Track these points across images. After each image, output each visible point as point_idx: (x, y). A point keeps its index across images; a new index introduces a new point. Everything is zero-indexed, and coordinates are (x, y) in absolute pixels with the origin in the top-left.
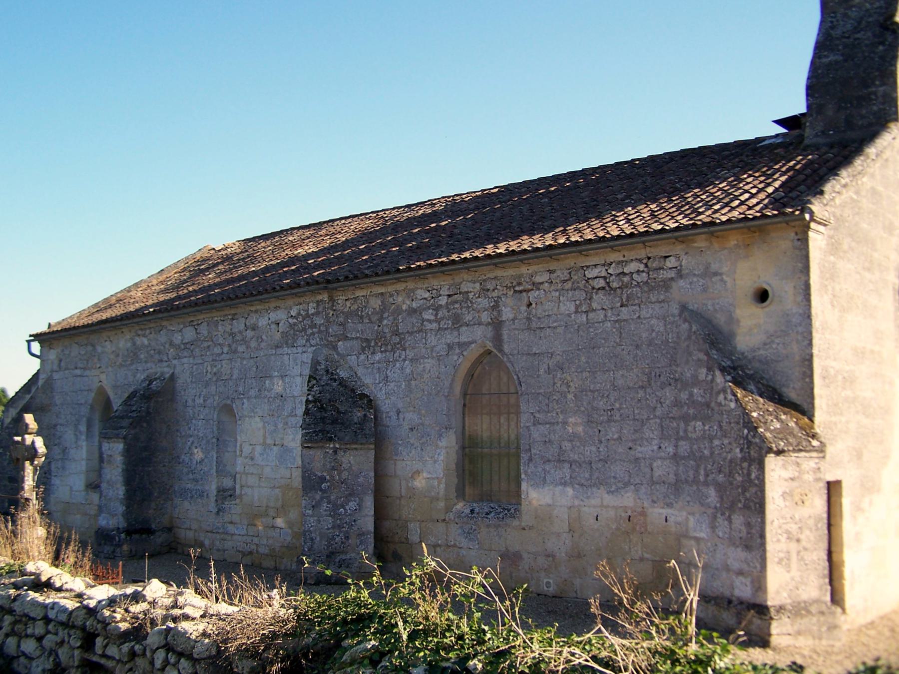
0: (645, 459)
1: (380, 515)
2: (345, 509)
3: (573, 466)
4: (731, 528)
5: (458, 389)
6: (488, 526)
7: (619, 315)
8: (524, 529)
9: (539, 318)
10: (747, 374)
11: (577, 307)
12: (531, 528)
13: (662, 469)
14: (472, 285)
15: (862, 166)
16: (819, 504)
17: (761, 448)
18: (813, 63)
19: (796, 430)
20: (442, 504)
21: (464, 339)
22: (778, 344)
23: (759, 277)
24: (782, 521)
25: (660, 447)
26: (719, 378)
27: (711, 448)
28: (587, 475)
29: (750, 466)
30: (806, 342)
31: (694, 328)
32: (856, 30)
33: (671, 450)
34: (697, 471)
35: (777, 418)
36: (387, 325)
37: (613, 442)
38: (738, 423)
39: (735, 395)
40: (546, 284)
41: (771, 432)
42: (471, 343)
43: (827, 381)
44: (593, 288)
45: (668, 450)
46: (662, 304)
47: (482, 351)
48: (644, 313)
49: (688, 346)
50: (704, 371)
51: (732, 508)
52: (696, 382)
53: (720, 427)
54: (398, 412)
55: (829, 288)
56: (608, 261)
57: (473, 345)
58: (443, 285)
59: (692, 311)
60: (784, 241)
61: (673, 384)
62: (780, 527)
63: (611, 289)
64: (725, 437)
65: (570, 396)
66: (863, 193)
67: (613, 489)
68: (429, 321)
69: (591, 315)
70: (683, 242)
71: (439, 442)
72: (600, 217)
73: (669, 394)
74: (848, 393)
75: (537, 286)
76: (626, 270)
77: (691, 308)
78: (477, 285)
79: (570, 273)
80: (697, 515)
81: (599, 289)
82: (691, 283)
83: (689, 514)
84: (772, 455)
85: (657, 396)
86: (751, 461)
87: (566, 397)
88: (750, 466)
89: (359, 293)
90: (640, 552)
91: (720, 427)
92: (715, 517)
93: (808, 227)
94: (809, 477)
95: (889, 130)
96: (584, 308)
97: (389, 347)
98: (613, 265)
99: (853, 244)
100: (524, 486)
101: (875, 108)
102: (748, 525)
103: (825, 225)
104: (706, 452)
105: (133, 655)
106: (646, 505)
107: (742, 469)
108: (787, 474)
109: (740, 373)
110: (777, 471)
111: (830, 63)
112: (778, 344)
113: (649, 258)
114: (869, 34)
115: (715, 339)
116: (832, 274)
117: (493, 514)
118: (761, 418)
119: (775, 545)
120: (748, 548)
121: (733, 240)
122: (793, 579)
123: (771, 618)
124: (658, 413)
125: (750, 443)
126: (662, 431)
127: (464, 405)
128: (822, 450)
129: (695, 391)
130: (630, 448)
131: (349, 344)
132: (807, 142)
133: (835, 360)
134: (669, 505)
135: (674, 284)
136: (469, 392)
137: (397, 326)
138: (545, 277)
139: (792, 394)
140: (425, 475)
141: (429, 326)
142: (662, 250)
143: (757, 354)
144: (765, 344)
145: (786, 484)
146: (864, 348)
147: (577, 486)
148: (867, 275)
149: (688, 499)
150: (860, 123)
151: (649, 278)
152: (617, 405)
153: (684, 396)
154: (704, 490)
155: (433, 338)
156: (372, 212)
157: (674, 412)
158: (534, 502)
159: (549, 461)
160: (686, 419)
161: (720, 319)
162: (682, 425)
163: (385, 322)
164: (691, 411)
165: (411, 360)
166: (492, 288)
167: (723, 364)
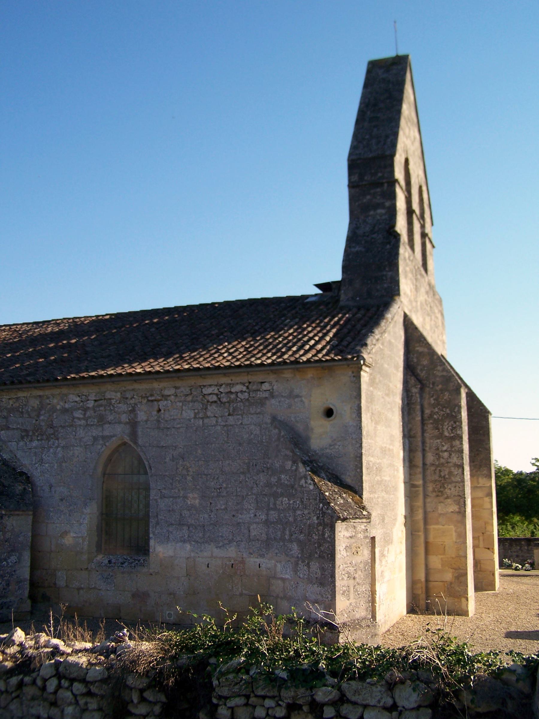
0: (244, 523)
1: (33, 567)
2: (7, 562)
3: (191, 529)
4: (309, 571)
5: (100, 470)
6: (123, 573)
7: (227, 421)
8: (152, 574)
9: (166, 421)
10: (319, 466)
11: (195, 414)
12: (157, 573)
13: (256, 531)
14: (114, 394)
15: (385, 326)
16: (366, 553)
17: (332, 517)
18: (346, 251)
19: (353, 504)
20: (85, 557)
21: (106, 433)
22: (339, 446)
23: (327, 400)
24: (344, 566)
25: (255, 515)
26: (302, 469)
27: (295, 516)
28: (201, 535)
29: (324, 529)
30: (358, 445)
31: (282, 433)
32: (372, 232)
33: (263, 517)
34: (283, 533)
35: (340, 496)
36: (43, 420)
37: (221, 511)
38: (315, 500)
39: (313, 480)
40: (173, 397)
41: (338, 505)
42: (112, 437)
43: (369, 471)
44: (208, 401)
45: (261, 517)
46: (259, 415)
47: (120, 442)
48: (245, 421)
49: (277, 446)
50: (290, 463)
51: (310, 557)
52: (283, 470)
53: (302, 502)
54: (51, 486)
55: (370, 408)
56: (220, 383)
57: (114, 438)
58: (92, 393)
59: (280, 421)
60: (344, 376)
61: (265, 471)
62: (344, 570)
63: (221, 402)
64: (306, 509)
65: (189, 478)
66: (385, 344)
67: (220, 545)
68: (79, 419)
69: (206, 421)
70: (275, 373)
71: (84, 510)
72: (205, 348)
73: (262, 478)
74: (378, 478)
75: (166, 397)
76: (233, 390)
77: (279, 418)
78: (119, 395)
79: (191, 390)
80: (283, 563)
81: (212, 402)
82: (279, 402)
83: (277, 562)
84: (340, 522)
85: (254, 479)
86: (325, 525)
87: (186, 479)
88: (324, 529)
89: (20, 394)
90: (240, 590)
91: (302, 502)
92: (297, 564)
93: (361, 369)
94: (360, 536)
95: (396, 302)
96: (201, 415)
97: (45, 437)
98: (224, 386)
99: (381, 378)
100: (152, 543)
101: (385, 285)
102: (323, 569)
103: (369, 367)
104: (291, 519)
105: (21, 685)
106: (245, 556)
107: (318, 530)
108: (348, 534)
109: (315, 465)
110: (343, 533)
111: (357, 252)
112: (339, 446)
113: (250, 383)
114: (380, 236)
115: (297, 441)
116: (371, 400)
117: (126, 564)
118: (331, 496)
119: (341, 582)
120: (322, 584)
121: (310, 374)
122: (351, 604)
123: (339, 632)
124: (254, 492)
125: (324, 513)
126: (257, 503)
127: (103, 482)
128: (369, 517)
129: (283, 476)
130: (234, 516)
131: (10, 433)
132: (342, 303)
133: (372, 456)
134: (262, 556)
135: (268, 402)
136: (107, 472)
137: (52, 421)
138: (172, 391)
139: (349, 480)
140: (72, 534)
141: (78, 423)
142: (260, 378)
143: (325, 452)
144: (330, 446)
145: (347, 540)
146: (386, 447)
147: (193, 543)
148: (387, 399)
149: (277, 551)
150: (376, 294)
151: (250, 397)
152: (225, 485)
153: (274, 480)
154: (289, 545)
155: (81, 431)
156: (5, 325)
157: (266, 491)
158: (161, 555)
159: (172, 524)
160: (276, 496)
161: (300, 427)
162: (272, 499)
163: (42, 417)
164: (279, 490)
165: (63, 447)
166: (130, 397)
167: (304, 458)
